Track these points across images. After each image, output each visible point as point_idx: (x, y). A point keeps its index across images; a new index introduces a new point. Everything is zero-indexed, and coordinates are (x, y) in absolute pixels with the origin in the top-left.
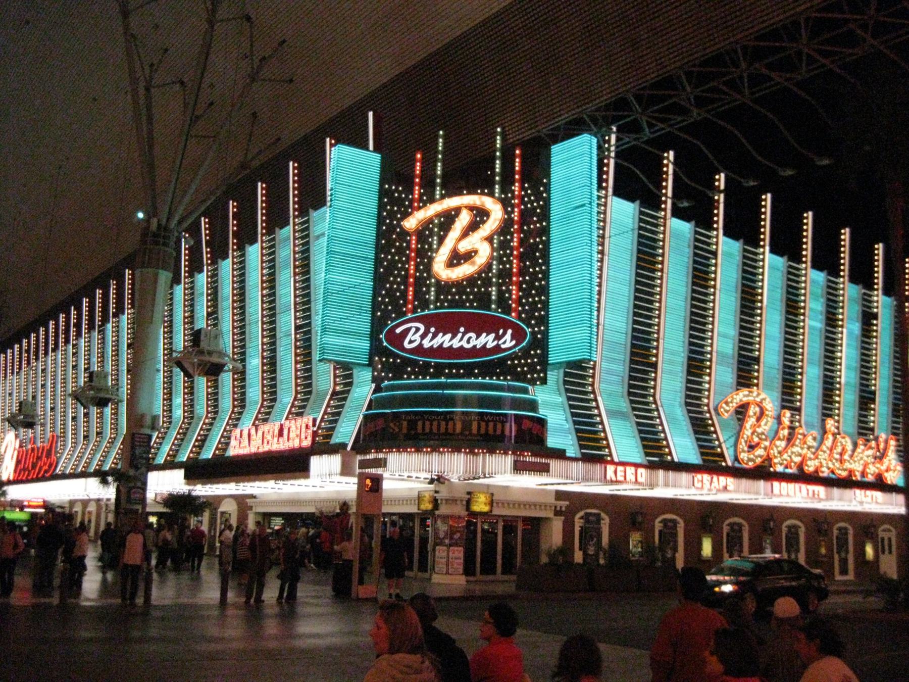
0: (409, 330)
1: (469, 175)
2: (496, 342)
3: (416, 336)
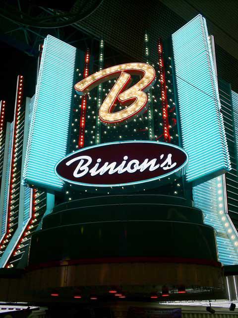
2: (158, 166)
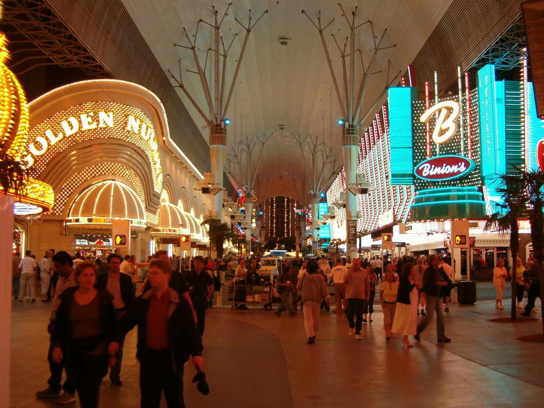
0: (424, 167)
1: (449, 90)
3: (428, 170)
